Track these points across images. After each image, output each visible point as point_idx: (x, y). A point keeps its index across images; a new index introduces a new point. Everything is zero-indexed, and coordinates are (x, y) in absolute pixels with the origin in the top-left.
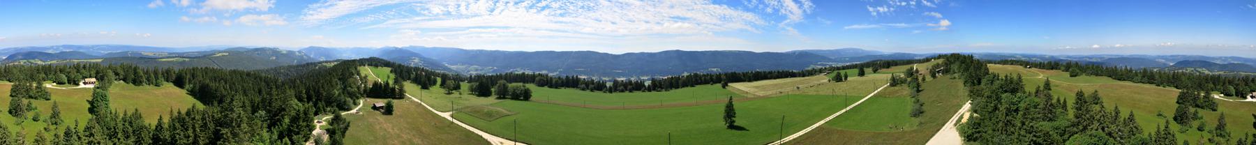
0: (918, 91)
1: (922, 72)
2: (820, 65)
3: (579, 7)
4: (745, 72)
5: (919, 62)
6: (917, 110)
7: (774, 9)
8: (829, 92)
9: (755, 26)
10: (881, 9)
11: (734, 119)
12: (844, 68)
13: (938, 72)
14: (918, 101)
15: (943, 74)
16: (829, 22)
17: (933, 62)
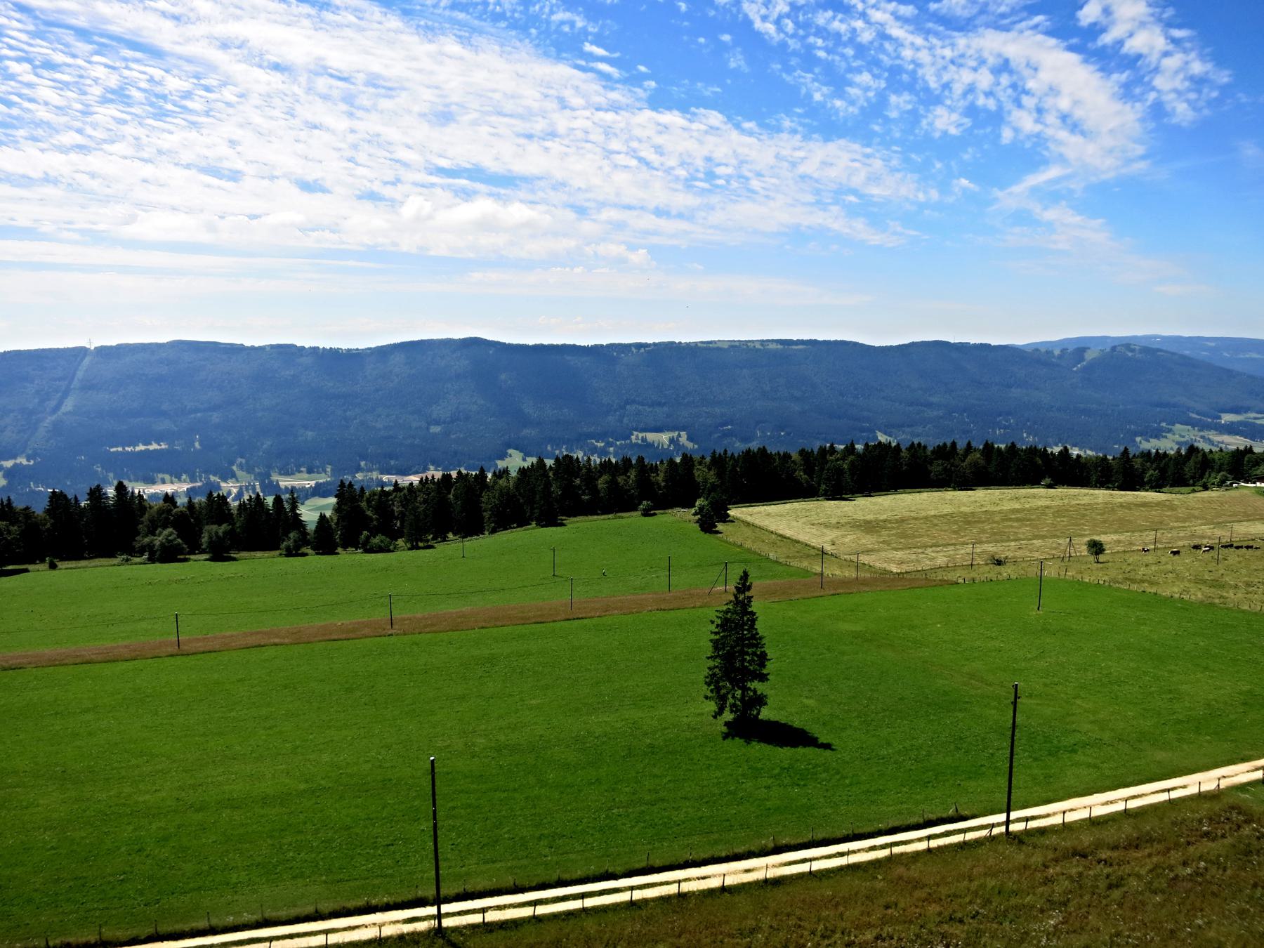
2: (1231, 429)
3: (97, 91)
7: (971, 111)
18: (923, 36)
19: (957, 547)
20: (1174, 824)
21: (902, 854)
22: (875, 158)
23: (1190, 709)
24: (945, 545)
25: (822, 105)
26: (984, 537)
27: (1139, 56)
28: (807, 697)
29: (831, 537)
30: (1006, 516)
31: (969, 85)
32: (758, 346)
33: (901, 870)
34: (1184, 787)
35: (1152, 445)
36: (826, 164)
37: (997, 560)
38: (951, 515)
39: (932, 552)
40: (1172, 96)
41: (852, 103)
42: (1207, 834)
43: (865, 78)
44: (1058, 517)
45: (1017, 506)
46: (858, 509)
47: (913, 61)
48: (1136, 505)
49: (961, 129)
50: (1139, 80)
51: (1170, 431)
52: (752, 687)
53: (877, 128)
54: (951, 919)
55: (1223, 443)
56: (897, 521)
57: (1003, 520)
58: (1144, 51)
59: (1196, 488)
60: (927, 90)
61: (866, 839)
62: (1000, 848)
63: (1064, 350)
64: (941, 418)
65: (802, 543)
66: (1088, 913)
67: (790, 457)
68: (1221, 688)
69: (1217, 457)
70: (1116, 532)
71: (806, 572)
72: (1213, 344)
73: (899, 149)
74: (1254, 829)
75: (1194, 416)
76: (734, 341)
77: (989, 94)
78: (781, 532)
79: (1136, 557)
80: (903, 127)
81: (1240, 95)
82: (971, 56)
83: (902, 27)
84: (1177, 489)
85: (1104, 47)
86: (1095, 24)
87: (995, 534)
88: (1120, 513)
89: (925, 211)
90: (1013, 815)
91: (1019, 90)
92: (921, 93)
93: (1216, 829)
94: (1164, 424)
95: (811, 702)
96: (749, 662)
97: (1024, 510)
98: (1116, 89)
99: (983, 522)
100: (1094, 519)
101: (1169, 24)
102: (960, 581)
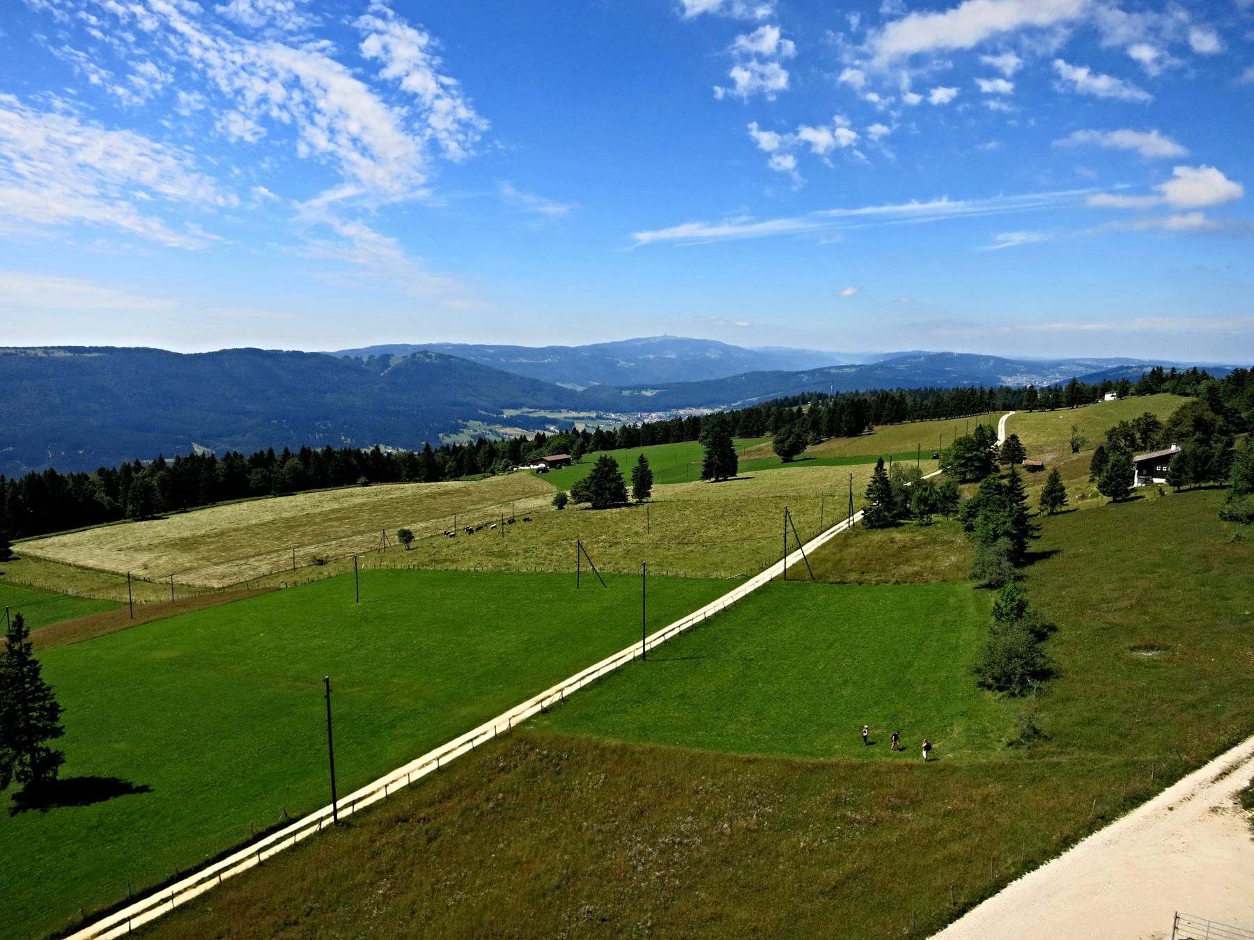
0: (1021, 557)
1: (1047, 458)
2: (511, 422)
4: (116, 463)
5: (1026, 400)
6: (1011, 655)
7: (265, 120)
8: (562, 559)
9: (156, 206)
10: (819, 138)
11: (51, 744)
12: (631, 438)
13: (1148, 469)
14: (1021, 607)
15: (1175, 480)
16: (556, 210)
17: (1137, 407)
18: (212, 36)
19: (280, 553)
20: (477, 768)
21: (232, 877)
22: (166, 154)
23: (486, 665)
24: (268, 553)
25: (99, 89)
26: (306, 540)
27: (415, 95)
28: (116, 741)
29: (142, 561)
30: (327, 517)
31: (262, 94)
32: (40, 354)
33: (233, 895)
34: (485, 733)
35: (449, 440)
36: (108, 154)
37: (319, 561)
38: (273, 522)
39: (256, 561)
40: (445, 135)
41: (137, 92)
42: (503, 769)
43: (149, 68)
44: (374, 512)
45: (336, 506)
46: (172, 526)
47: (202, 61)
48: (440, 494)
49: (257, 137)
50: (417, 116)
51: (465, 427)
52: (44, 747)
53: (166, 124)
54: (286, 925)
55: (506, 434)
56: (216, 535)
57: (324, 521)
58: (420, 91)
59: (486, 474)
60: (218, 92)
61: (192, 874)
62: (330, 838)
63: (371, 357)
64: (260, 425)
65: (108, 572)
66: (412, 871)
67: (87, 478)
68: (508, 642)
69: (500, 447)
70: (424, 520)
71: (114, 602)
72: (492, 351)
73: (192, 149)
74: (537, 754)
75: (483, 413)
76: (8, 348)
77: (282, 107)
78: (81, 563)
79: (441, 540)
80: (196, 127)
81: (497, 142)
82: (262, 66)
83: (188, 23)
84: (471, 477)
85: (385, 81)
86: (376, 58)
87: (317, 535)
88: (426, 502)
89: (226, 216)
90: (340, 804)
91: (311, 110)
92: (213, 95)
93: (510, 762)
94: (460, 421)
95: (121, 746)
96: (37, 719)
97: (343, 509)
98: (399, 121)
99: (305, 525)
100: (406, 511)
101: (438, 71)
102: (283, 586)
